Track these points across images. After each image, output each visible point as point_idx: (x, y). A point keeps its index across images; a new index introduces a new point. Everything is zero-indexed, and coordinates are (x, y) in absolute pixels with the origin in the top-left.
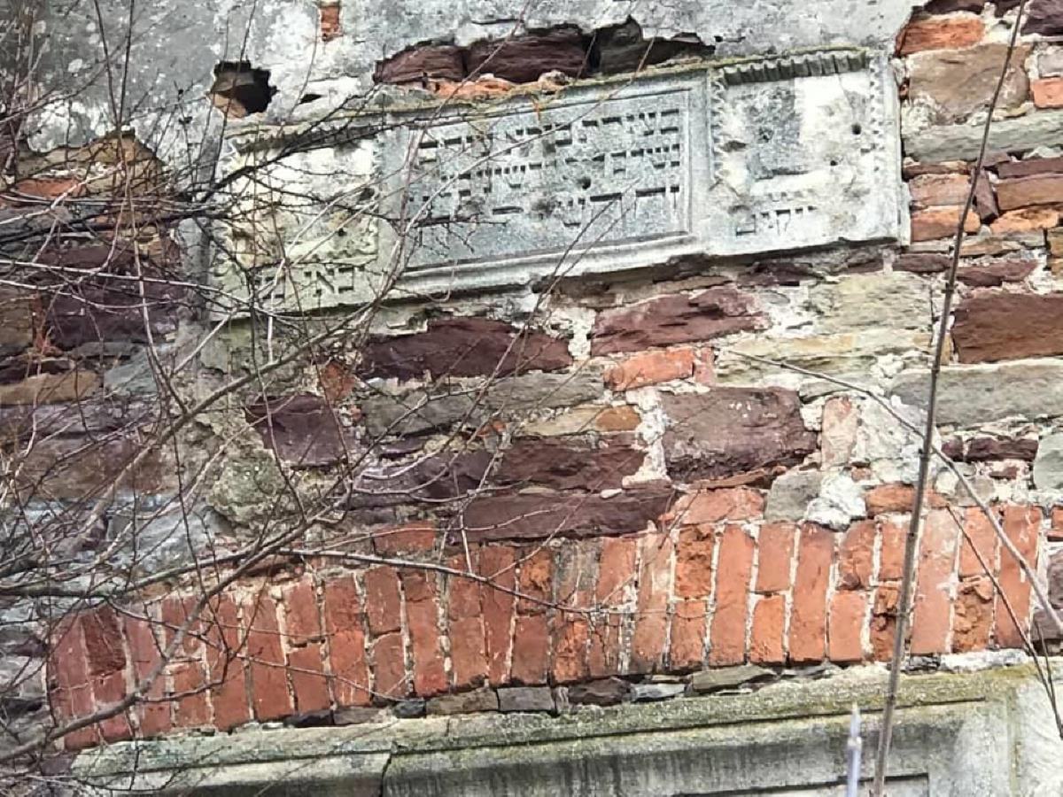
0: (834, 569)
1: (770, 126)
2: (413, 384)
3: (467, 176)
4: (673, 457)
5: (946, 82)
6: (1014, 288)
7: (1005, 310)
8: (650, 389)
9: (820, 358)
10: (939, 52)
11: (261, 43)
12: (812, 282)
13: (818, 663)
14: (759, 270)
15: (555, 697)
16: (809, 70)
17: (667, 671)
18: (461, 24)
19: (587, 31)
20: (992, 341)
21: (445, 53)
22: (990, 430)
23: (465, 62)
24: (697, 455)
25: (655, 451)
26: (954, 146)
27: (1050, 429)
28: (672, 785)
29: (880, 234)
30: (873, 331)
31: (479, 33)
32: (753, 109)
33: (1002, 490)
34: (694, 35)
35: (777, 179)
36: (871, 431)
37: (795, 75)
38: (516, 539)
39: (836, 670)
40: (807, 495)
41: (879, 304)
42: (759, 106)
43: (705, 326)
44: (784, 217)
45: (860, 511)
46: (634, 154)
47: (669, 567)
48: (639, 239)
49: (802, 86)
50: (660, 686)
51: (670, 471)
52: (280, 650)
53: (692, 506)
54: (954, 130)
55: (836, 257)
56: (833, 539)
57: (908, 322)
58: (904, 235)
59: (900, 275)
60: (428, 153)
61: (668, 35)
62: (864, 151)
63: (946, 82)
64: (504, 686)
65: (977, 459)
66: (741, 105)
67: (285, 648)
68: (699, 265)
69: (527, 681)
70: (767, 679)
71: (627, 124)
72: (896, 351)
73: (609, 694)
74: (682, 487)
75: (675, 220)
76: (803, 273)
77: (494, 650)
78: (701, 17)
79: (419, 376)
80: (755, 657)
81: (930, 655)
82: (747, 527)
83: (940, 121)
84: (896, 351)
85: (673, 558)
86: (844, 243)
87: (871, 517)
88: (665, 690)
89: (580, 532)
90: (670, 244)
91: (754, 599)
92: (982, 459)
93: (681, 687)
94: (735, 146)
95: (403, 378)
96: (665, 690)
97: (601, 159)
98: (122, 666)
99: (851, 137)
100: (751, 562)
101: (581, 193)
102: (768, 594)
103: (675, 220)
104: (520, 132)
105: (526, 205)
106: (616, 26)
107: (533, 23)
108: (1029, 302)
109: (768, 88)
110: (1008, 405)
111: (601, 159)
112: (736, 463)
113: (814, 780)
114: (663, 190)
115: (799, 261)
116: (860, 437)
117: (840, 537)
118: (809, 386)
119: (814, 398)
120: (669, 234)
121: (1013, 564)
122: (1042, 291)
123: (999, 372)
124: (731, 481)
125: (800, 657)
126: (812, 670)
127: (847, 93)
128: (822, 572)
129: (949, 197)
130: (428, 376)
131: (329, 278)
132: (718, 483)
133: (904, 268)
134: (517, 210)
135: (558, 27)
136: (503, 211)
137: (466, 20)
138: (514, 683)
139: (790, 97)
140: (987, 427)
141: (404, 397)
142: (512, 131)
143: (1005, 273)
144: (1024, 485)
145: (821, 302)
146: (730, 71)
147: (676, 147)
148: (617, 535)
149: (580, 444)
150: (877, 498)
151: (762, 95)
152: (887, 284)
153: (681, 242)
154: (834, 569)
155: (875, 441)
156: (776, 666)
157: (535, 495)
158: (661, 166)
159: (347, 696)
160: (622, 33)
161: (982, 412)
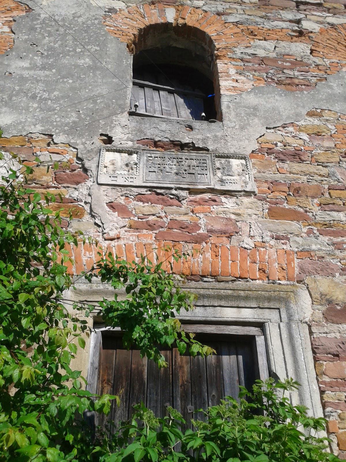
2: (146, 204)
3: (159, 164)
5: (260, 165)
8: (202, 214)
13: (247, 278)
17: (211, 276)
23: (156, 144)
24: (214, 229)
25: (203, 227)
29: (252, 190)
32: (221, 163)
33: (285, 247)
46: (197, 166)
49: (231, 160)
53: (213, 240)
55: (242, 193)
63: (260, 165)
70: (235, 280)
71: (195, 161)
75: (207, 180)
78: (208, 144)
80: (232, 275)
83: (260, 172)
86: (244, 191)
88: (211, 280)
90: (206, 185)
92: (279, 239)
93: (214, 280)
95: (144, 202)
96: (211, 280)
97: (189, 166)
101: (184, 172)
102: (233, 262)
103: (207, 180)
108: (284, 209)
110: (283, 229)
112: (223, 233)
113: (252, 306)
117: (249, 251)
119: (239, 221)
126: (245, 280)
128: (246, 258)
130: (150, 203)
131: (128, 179)
135: (176, 141)
137: (156, 136)
141: (144, 207)
145: (239, 203)
148: (196, 243)
149: (187, 223)
151: (223, 161)
152: (253, 201)
153: (208, 185)
156: (237, 278)
158: (203, 170)
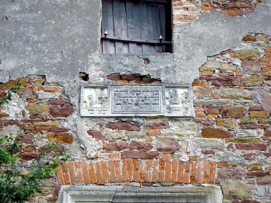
0: (184, 168)
1: (173, 95)
2: (115, 130)
4: (158, 148)
6: (211, 127)
7: (210, 130)
9: (221, 151)
10: (198, 87)
11: (87, 69)
12: (179, 122)
13: (182, 183)
14: (171, 119)
15: (140, 184)
16: (179, 87)
17: (158, 182)
18: (121, 71)
19: (142, 75)
20: (208, 135)
21: (118, 75)
22: (208, 149)
23: (121, 77)
24: (162, 148)
26: (201, 103)
27: (217, 150)
28: (161, 201)
29: (191, 116)
30: (189, 131)
31: (124, 73)
33: (210, 159)
34: (159, 78)
35: (174, 105)
36: (190, 147)
37: (176, 88)
38: (133, 158)
39: (185, 185)
40: (179, 156)
41: (190, 127)
42: (171, 92)
43: (162, 126)
44: (176, 111)
45: (188, 160)
47: (158, 165)
48: (152, 112)
50: (157, 184)
51: (157, 150)
52: (94, 172)
53: (161, 155)
54: (201, 100)
55: (184, 118)
56: (184, 164)
57: (194, 130)
58: (194, 115)
59: (193, 123)
60: (117, 93)
61: (155, 78)
62: (188, 102)
63: (200, 92)
64: (132, 182)
65: (206, 153)
66: (168, 91)
67: (95, 172)
68: (162, 117)
69: (135, 181)
70: (174, 185)
71: (150, 92)
72: (193, 135)
73: (149, 185)
74: (160, 153)
76: (178, 120)
77: (130, 176)
79: (116, 129)
81: (200, 184)
82: (170, 160)
84: (193, 135)
85: (159, 164)
87: (190, 161)
88: (158, 185)
89: (144, 158)
91: (172, 172)
93: (160, 185)
94: (167, 98)
95: (113, 129)
97: (146, 97)
98: (68, 171)
99: (185, 99)
100: (171, 166)
101: (142, 103)
104: (132, 91)
105: (133, 103)
106: (146, 75)
107: (133, 73)
108: (214, 129)
109: (172, 89)
110: (211, 145)
111: (146, 97)
114: (156, 104)
115: (177, 119)
116: (188, 148)
118: (179, 139)
120: (157, 111)
121: (211, 171)
122: (215, 128)
123: (209, 140)
124: (167, 152)
125: (179, 182)
127: (185, 92)
128: (183, 169)
129: (201, 111)
132: (165, 153)
133: (194, 121)
134: (132, 104)
135: (137, 74)
136: (130, 104)
138: (133, 181)
139: (176, 92)
140: (207, 148)
142: (131, 91)
143: (210, 124)
144: (213, 158)
145: (181, 125)
146: (167, 86)
147: (158, 97)
150: (191, 158)
151: (171, 90)
152: (191, 123)
153: (159, 113)
154: (184, 168)
155: (190, 149)
157: (136, 151)
158: (156, 100)
159: (106, 181)
160: (147, 76)
161: (207, 146)
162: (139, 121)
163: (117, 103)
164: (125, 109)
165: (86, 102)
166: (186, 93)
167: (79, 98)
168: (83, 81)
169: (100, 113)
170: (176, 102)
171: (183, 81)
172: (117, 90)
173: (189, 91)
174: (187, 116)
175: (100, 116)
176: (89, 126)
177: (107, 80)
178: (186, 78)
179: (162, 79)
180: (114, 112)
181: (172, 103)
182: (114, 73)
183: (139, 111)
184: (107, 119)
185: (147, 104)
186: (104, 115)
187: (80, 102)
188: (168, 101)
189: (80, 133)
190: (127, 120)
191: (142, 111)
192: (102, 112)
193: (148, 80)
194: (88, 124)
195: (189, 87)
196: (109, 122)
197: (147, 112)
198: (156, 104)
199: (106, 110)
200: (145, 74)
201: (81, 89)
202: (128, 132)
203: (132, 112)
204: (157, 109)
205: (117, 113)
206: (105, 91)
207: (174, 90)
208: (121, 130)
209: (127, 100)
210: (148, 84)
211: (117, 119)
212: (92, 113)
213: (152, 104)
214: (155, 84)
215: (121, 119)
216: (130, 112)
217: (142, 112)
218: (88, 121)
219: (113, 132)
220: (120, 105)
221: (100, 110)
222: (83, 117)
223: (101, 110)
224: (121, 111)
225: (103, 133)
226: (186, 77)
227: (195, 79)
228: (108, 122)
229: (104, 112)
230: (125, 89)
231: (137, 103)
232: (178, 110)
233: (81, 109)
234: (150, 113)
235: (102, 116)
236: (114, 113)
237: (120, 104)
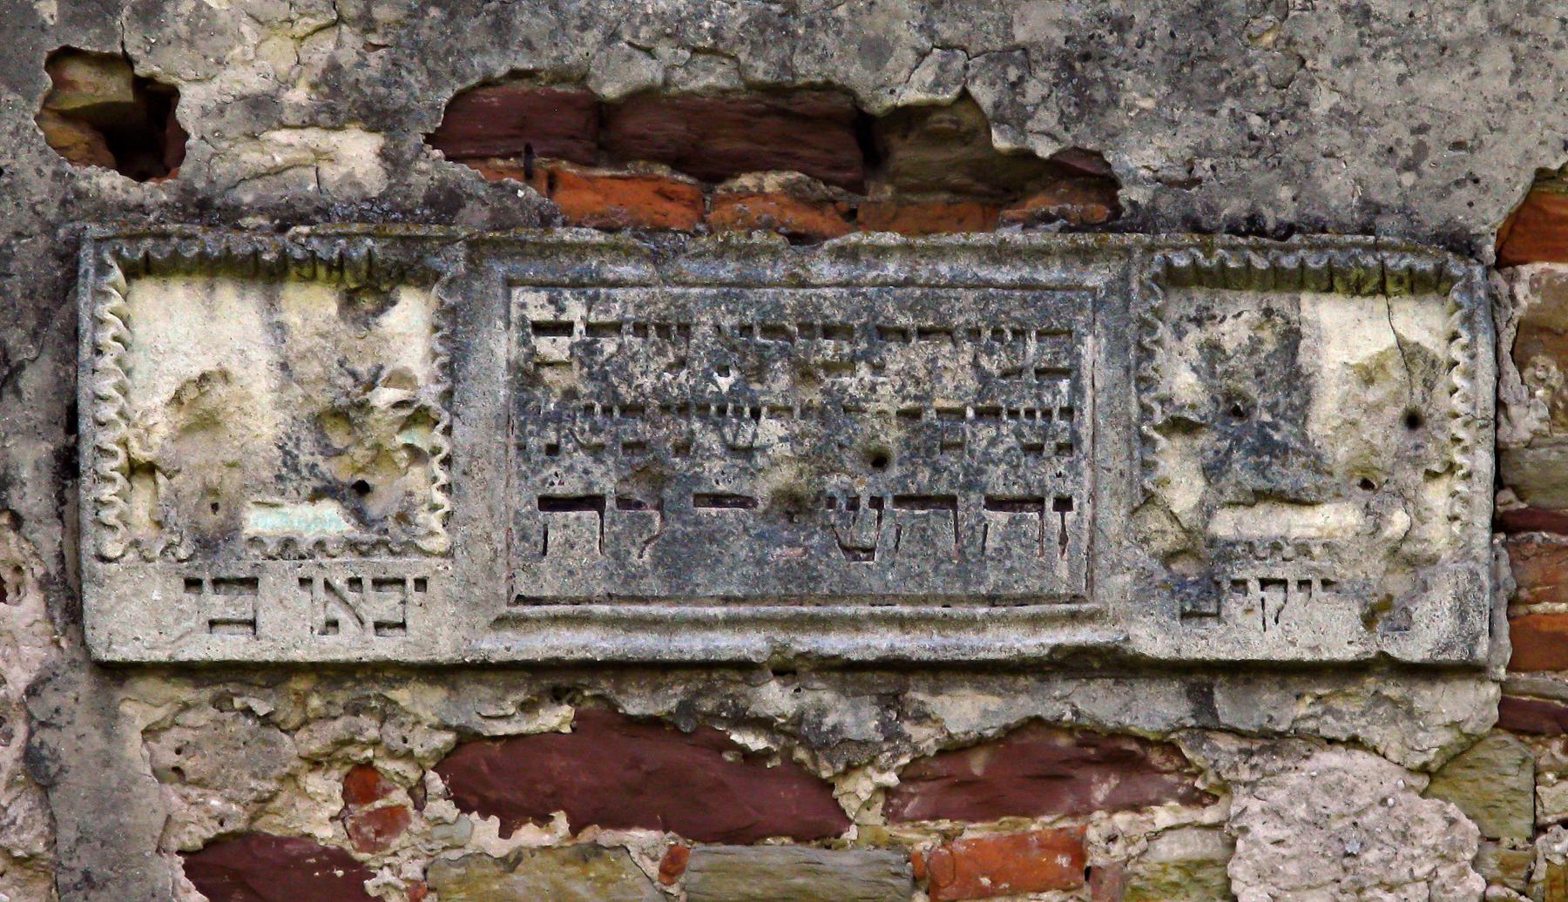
2: (529, 835)
21: (566, 100)
23: (602, 130)
29: (1455, 656)
31: (646, 72)
34: (1099, 155)
35: (1261, 509)
37: (1301, 286)
42: (1229, 345)
44: (1274, 597)
48: (992, 600)
62: (1432, 476)
79: (543, 820)
94: (1179, 426)
106: (934, 107)
120: (1054, 599)
127: (1401, 343)
135: (812, 86)
136: (717, 500)
139: (1291, 338)
146: (1181, 261)
147: (1067, 412)
153: (1074, 617)
158: (1036, 450)
160: (942, 121)
162: (830, 721)
163: (558, 490)
164: (658, 562)
165: (150, 469)
166: (1409, 353)
167: (59, 410)
168: (109, 182)
169: (341, 615)
170: (1285, 484)
171: (1392, 198)
172: (547, 315)
173: (1454, 337)
174: (1414, 650)
175: (341, 656)
176: (199, 783)
177: (431, 168)
178: (1433, 156)
179: (1140, 159)
180: (521, 600)
181: (1229, 495)
182: (515, 74)
183: (833, 598)
184: (423, 702)
185: (922, 500)
186: (387, 648)
187: (67, 466)
188: (1193, 465)
189: (87, 876)
190: (686, 708)
191: (858, 598)
192: (363, 610)
193: (953, 166)
194: (188, 764)
195: (1453, 280)
196: (459, 730)
197: (925, 600)
198: (1039, 502)
199: (421, 584)
200: (912, 95)
201: (84, 299)
202: (702, 856)
203: (744, 610)
204: (1048, 567)
205: (555, 620)
206: (409, 320)
207: (1268, 313)
208: (608, 837)
209: (683, 449)
210: (945, 239)
211: (558, 696)
212: (231, 614)
213: (995, 503)
214: (1038, 238)
215: (605, 687)
216: (719, 611)
217: (864, 610)
218: (191, 717)
219: (510, 863)
220: (590, 515)
221: (339, 582)
222: (117, 673)
223: (355, 582)
224: (610, 598)
225: (386, 875)
226: (1429, 139)
227: (1542, 175)
228: (450, 737)
229: (384, 605)
230: (652, 301)
231: (803, 487)
232: (1304, 584)
233: (89, 563)
234: (969, 623)
235: (369, 655)
236: (520, 621)
237: (593, 502)
